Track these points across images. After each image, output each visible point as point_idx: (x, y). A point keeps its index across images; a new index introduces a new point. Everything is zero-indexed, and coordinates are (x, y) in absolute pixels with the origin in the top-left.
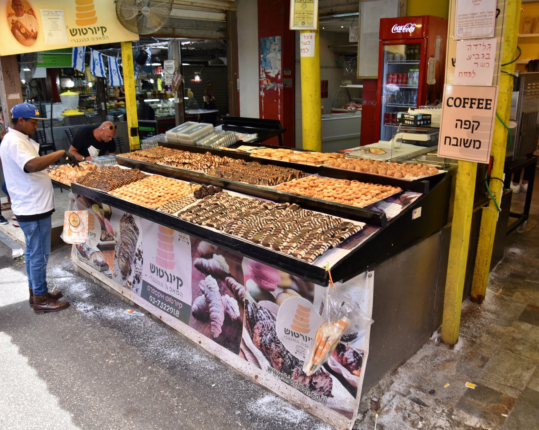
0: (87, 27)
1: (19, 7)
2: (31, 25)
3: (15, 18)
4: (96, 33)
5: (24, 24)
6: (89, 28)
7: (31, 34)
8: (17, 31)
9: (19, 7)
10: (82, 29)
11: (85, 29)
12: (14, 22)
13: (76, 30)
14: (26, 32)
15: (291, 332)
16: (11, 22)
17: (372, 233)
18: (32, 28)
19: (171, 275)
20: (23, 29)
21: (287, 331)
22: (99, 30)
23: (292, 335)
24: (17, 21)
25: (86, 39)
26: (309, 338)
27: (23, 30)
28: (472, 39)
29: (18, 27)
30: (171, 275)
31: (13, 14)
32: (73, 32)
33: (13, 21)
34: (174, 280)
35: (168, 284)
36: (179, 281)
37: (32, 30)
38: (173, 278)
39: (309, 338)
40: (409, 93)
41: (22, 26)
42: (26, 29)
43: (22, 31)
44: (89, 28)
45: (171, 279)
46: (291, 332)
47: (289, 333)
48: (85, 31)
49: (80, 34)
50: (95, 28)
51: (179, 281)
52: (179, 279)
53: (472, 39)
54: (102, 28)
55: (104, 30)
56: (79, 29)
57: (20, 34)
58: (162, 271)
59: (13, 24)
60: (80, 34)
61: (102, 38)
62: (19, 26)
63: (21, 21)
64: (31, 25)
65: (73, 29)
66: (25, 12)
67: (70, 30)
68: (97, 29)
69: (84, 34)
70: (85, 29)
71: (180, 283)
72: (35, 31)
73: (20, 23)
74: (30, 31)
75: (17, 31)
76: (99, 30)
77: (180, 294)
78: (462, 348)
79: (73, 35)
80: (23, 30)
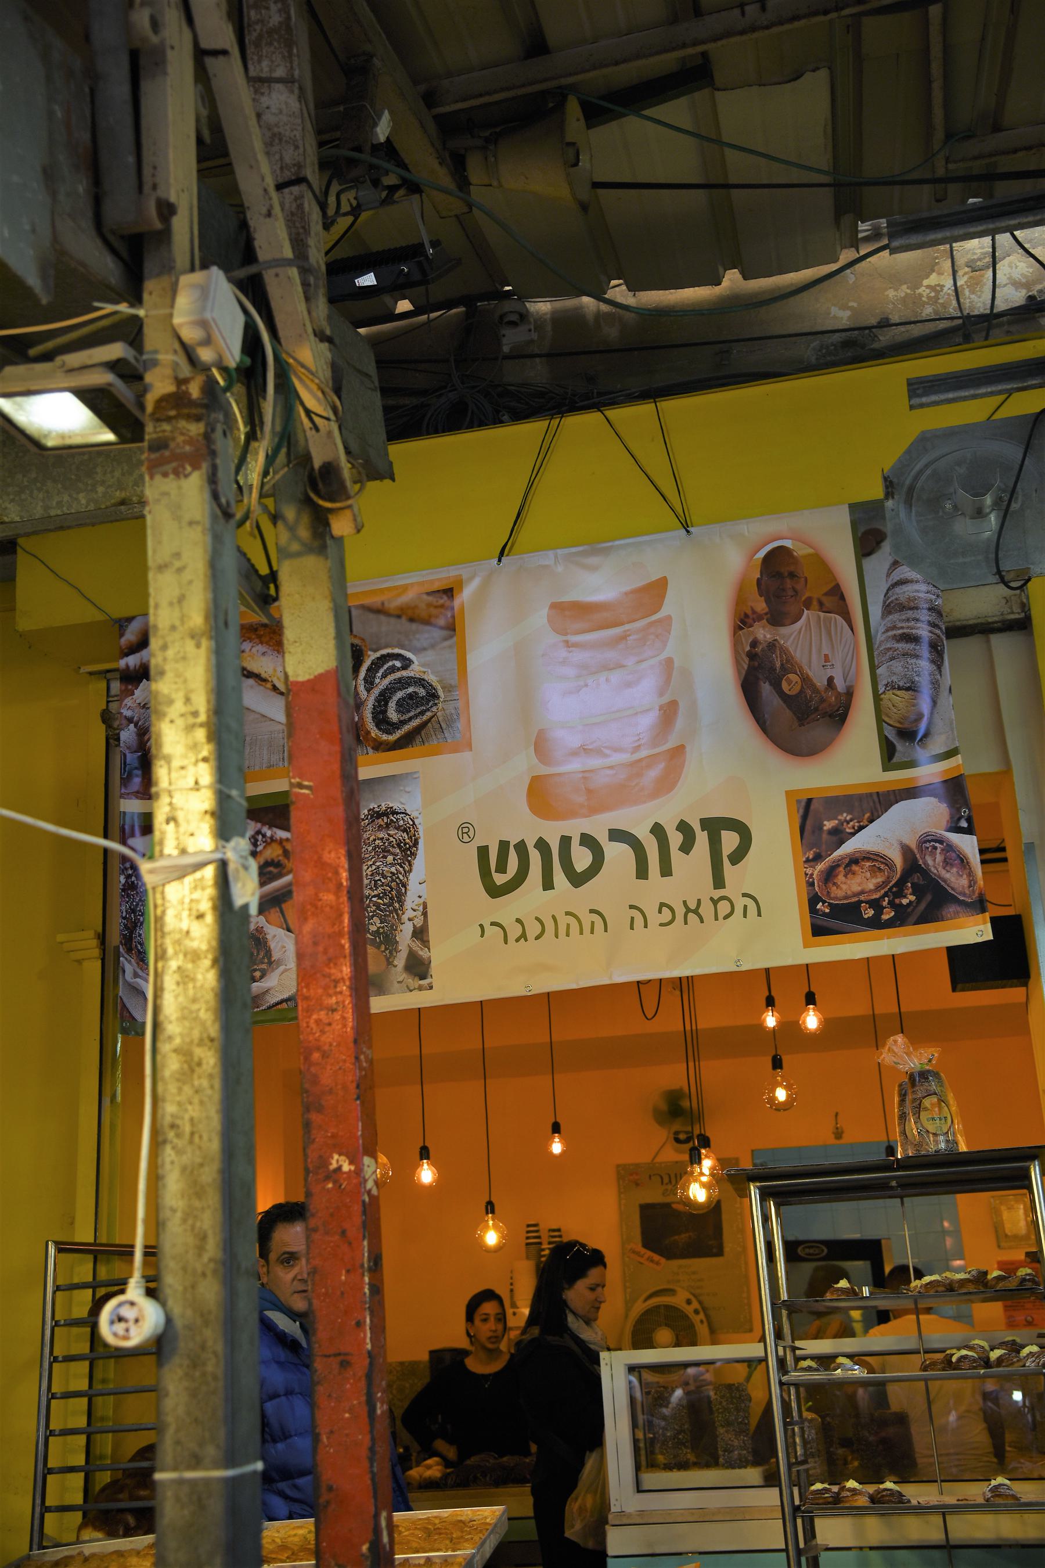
0: (598, 827)
1: (789, 583)
2: (827, 658)
3: (763, 633)
4: (666, 870)
5: (799, 655)
6: (616, 835)
7: (822, 700)
8: (766, 688)
9: (789, 583)
10: (565, 841)
11: (587, 840)
12: (758, 650)
13: (521, 848)
14: (801, 691)
15: (535, 858)
16: (748, 648)
18: (830, 673)
20: (792, 676)
22: (686, 847)
24: (772, 646)
25: (587, 919)
27: (791, 685)
29: (773, 669)
31: (760, 618)
32: (502, 868)
33: (754, 644)
37: (831, 680)
40: (279, 178)
41: (789, 666)
42: (806, 680)
43: (785, 686)
44: (616, 835)
48: (582, 859)
49: (548, 884)
50: (658, 830)
54: (714, 826)
55: (730, 840)
56: (542, 845)
57: (777, 701)
59: (752, 656)
60: (548, 884)
61: (707, 909)
62: (778, 665)
63: (789, 644)
64: (827, 658)
65: (504, 846)
66: (808, 604)
67: (483, 852)
68: (675, 839)
69: (578, 880)
70: (587, 840)
72: (840, 685)
73: (784, 651)
74: (821, 682)
75: (766, 688)
76: (686, 847)
77: (740, 903)
78: (157, 64)
79: (495, 891)
80: (791, 685)
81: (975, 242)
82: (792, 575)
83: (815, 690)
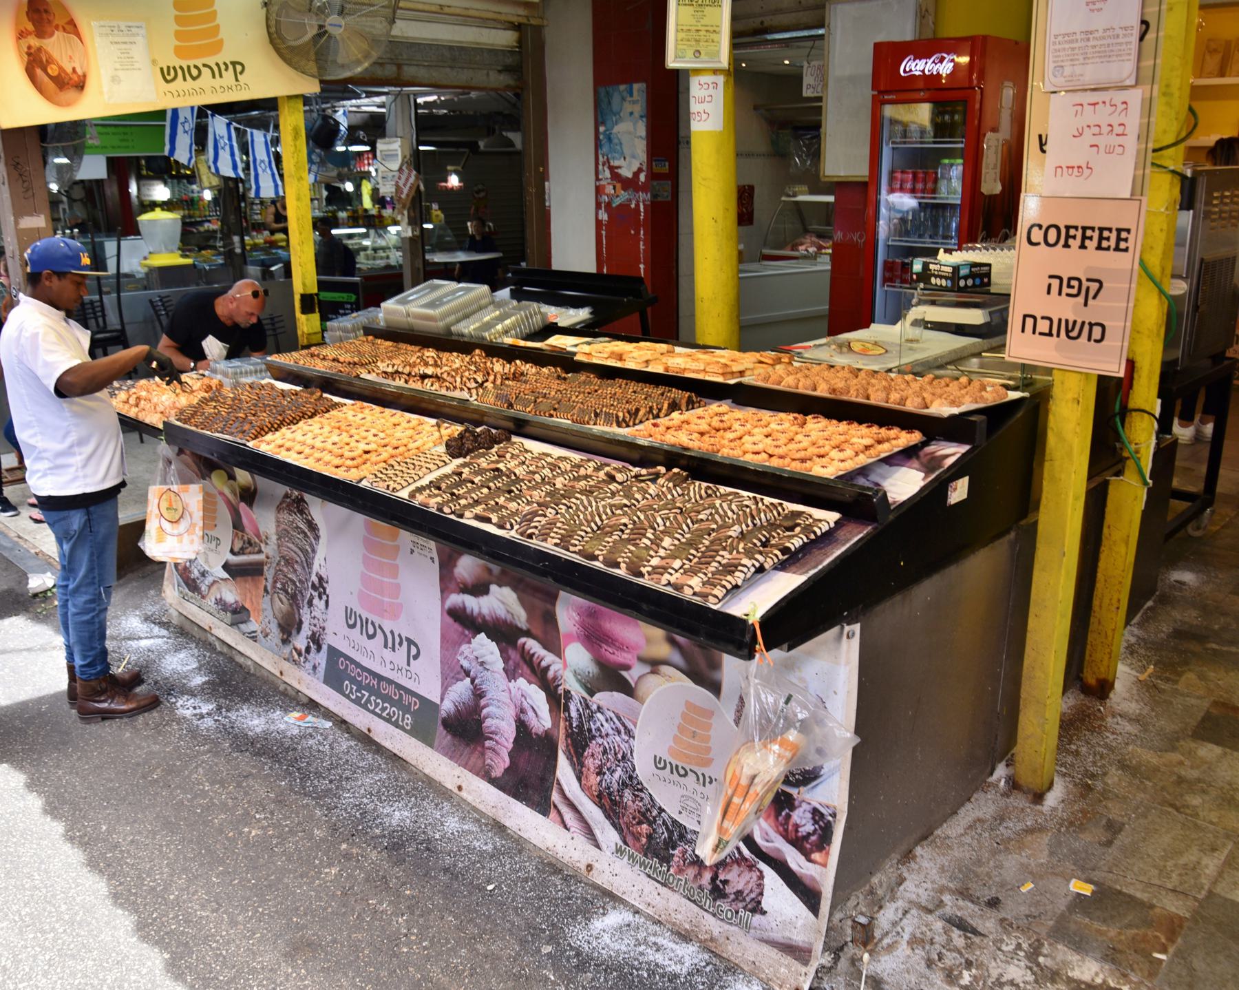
0: (199, 63)
1: (45, 16)
2: (71, 57)
4: (221, 76)
5: (55, 54)
6: (204, 65)
7: (71, 79)
8: (39, 72)
10: (189, 67)
11: (196, 67)
12: (32, 51)
13: (174, 68)
14: (59, 74)
15: (668, 765)
16: (26, 50)
17: (855, 536)
18: (73, 65)
19: (392, 632)
20: (53, 66)
21: (660, 763)
22: (227, 69)
23: (672, 772)
24: (39, 49)
25: (198, 90)
26: (710, 777)
27: (53, 70)
28: (1086, 90)
29: (41, 61)
30: (392, 632)
31: (30, 33)
32: (169, 74)
33: (29, 47)
34: (401, 644)
35: (387, 654)
36: (412, 647)
37: (74, 70)
38: (397, 640)
39: (710, 777)
41: (50, 60)
42: (60, 68)
43: (50, 71)
44: (204, 65)
45: (392, 642)
46: (668, 765)
47: (664, 768)
48: (195, 72)
49: (185, 79)
50: (217, 64)
51: (412, 647)
52: (410, 642)
53: (1086, 90)
54: (234, 64)
55: (239, 68)
56: (181, 68)
57: (46, 79)
58: (373, 624)
60: (185, 79)
61: (234, 88)
62: (44, 59)
63: (49, 49)
64: (71, 57)
65: (168, 68)
66: (57, 28)
67: (162, 69)
68: (223, 67)
69: (194, 78)
70: (196, 67)
71: (414, 651)
72: (79, 71)
73: (46, 52)
74: (69, 70)
75: (39, 72)
76: (227, 69)
77: (414, 676)
79: (167, 81)
80: (53, 70)
81: (957, 184)
82: (46, 11)
83: (67, 74)
